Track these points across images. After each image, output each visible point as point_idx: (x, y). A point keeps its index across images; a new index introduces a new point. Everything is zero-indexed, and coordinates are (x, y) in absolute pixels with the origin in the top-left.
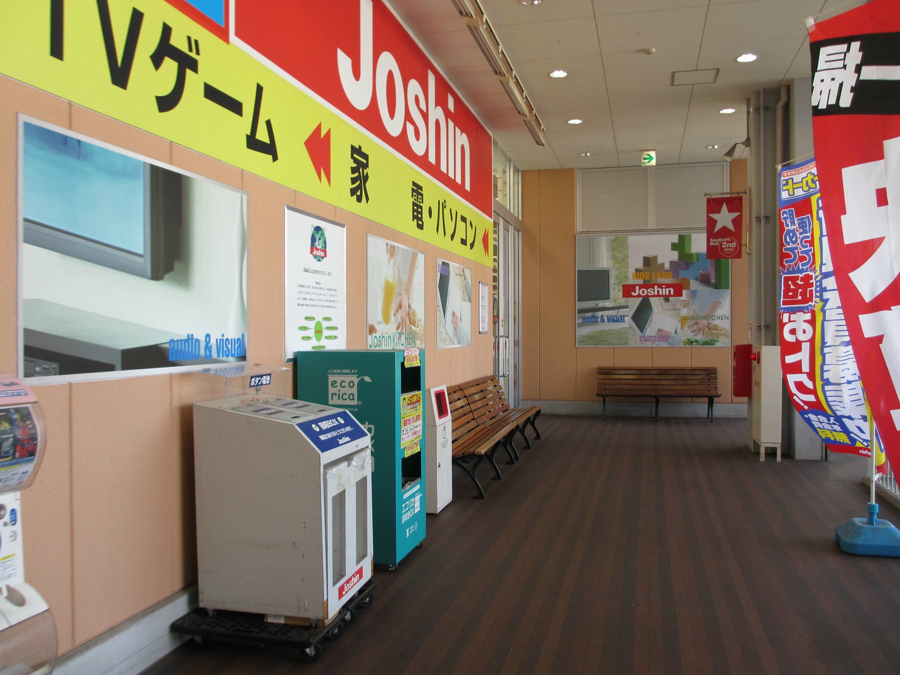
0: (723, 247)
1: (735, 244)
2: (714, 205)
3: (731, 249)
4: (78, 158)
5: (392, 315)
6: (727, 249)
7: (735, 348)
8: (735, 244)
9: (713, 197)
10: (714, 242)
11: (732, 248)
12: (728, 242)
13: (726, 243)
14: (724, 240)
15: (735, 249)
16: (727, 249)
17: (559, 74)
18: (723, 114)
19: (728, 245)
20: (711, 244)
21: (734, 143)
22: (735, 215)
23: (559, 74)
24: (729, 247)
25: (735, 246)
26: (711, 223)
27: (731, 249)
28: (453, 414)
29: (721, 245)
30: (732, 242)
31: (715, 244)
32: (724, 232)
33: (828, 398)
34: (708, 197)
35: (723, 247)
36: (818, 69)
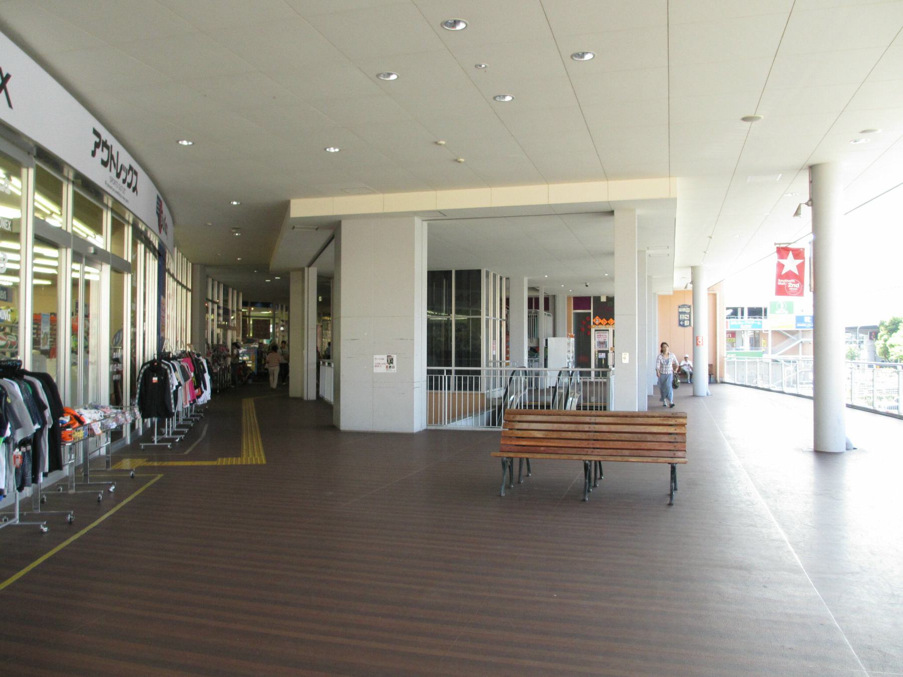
0: (789, 286)
1: (798, 284)
2: (783, 251)
3: (795, 289)
4: (18, 323)
5: (671, 387)
6: (792, 289)
7: (244, 307)
8: (798, 284)
9: (782, 246)
10: (782, 282)
11: (796, 288)
12: (793, 283)
13: (791, 284)
14: (789, 281)
15: (799, 289)
16: (792, 289)
17: (235, 203)
18: (159, 247)
19: (792, 284)
20: (779, 284)
21: (799, 204)
22: (799, 261)
23: (235, 203)
24: (794, 287)
25: (798, 286)
26: (780, 266)
27: (795, 289)
28: (525, 459)
29: (787, 285)
30: (796, 283)
31: (782, 284)
32: (790, 275)
33: (811, 393)
34: (778, 246)
35: (789, 286)
36: (105, 249)
